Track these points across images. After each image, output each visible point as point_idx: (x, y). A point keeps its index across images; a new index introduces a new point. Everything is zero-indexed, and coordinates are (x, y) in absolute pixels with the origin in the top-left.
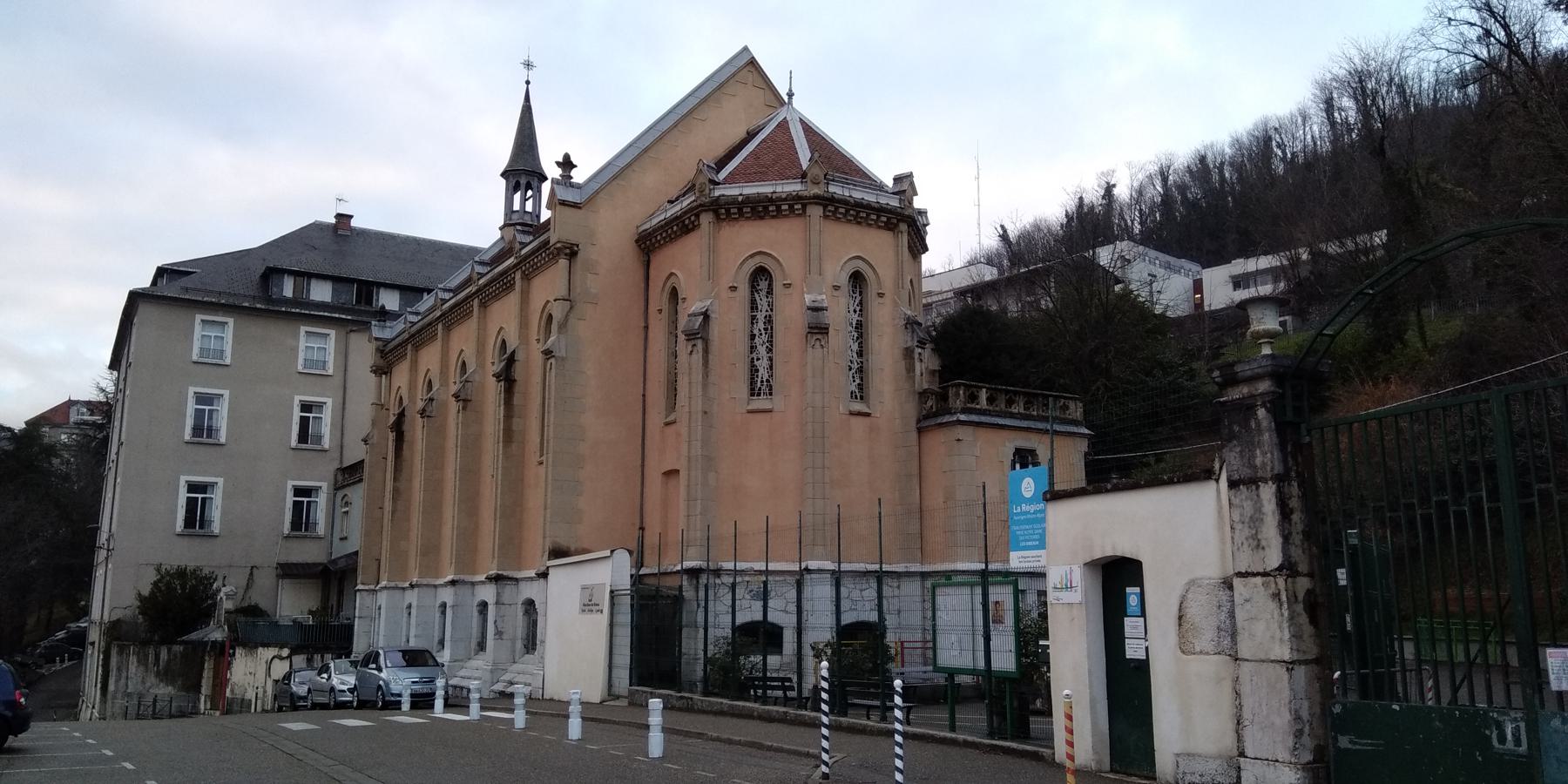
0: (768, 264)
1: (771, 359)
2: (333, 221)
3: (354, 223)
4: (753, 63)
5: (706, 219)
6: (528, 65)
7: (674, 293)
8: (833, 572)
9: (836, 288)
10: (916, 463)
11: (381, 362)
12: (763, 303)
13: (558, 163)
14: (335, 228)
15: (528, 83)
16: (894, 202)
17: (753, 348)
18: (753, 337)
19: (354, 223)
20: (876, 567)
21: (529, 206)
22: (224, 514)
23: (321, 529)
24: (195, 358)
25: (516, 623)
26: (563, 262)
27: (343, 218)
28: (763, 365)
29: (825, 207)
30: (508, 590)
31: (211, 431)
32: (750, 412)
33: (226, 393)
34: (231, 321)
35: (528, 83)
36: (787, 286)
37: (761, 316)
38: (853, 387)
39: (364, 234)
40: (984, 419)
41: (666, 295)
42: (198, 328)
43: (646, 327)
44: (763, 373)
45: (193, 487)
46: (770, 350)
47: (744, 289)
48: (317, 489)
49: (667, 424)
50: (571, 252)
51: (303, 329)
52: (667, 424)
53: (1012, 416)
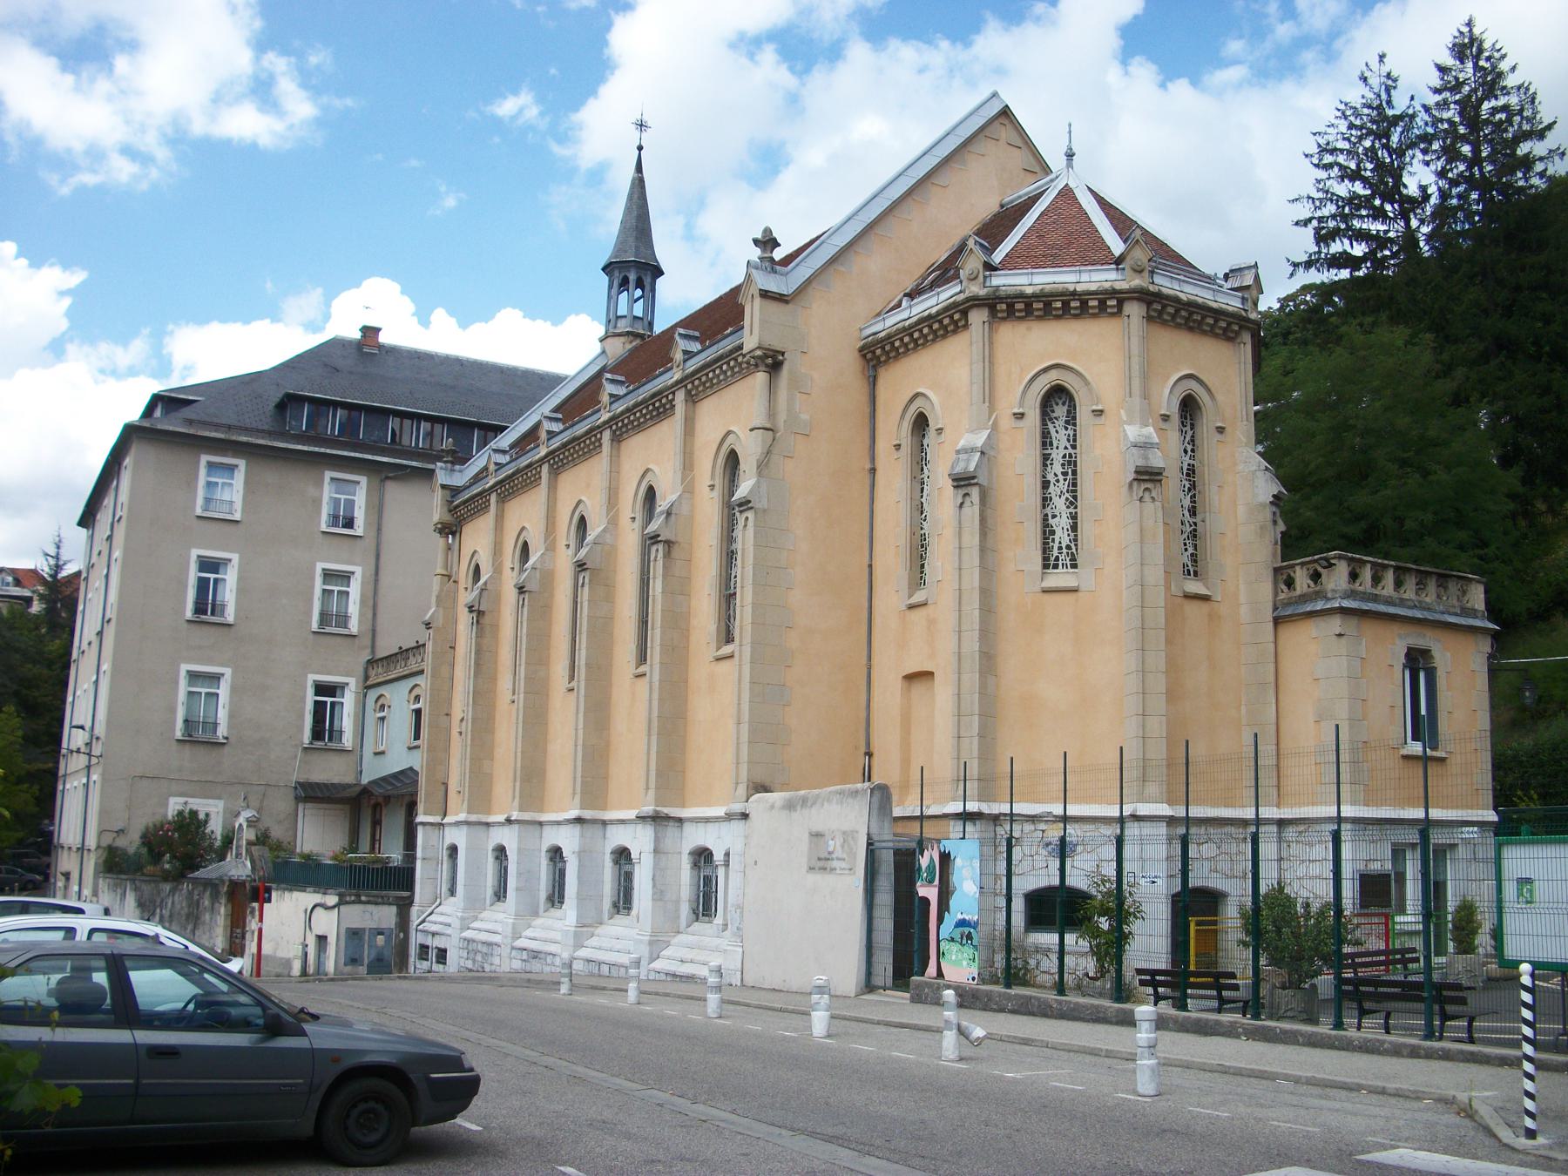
0: (1069, 381)
1: (1074, 517)
2: (358, 335)
3: (384, 338)
4: (1006, 112)
5: (978, 317)
6: (641, 126)
7: (921, 423)
8: (1171, 821)
9: (1165, 418)
10: (1272, 667)
11: (448, 518)
12: (1060, 436)
13: (756, 242)
14: (359, 346)
15: (640, 148)
16: (1233, 303)
17: (1046, 501)
18: (1045, 485)
19: (384, 338)
20: (1419, 813)
21: (638, 310)
22: (232, 716)
23: (348, 740)
24: (199, 512)
25: (684, 878)
26: (761, 377)
27: (370, 332)
28: (1061, 524)
29: (1149, 304)
30: (671, 831)
31: (217, 609)
32: (1045, 591)
33: (235, 557)
34: (242, 464)
35: (640, 148)
36: (1099, 413)
37: (1057, 455)
38: (1186, 559)
39: (393, 351)
40: (1392, 610)
41: (907, 425)
42: (203, 471)
43: (873, 470)
44: (1062, 537)
45: (194, 677)
46: (1072, 503)
47: (1034, 415)
48: (343, 686)
49: (912, 607)
50: (773, 362)
51: (328, 475)
52: (912, 607)
53: (1402, 603)
